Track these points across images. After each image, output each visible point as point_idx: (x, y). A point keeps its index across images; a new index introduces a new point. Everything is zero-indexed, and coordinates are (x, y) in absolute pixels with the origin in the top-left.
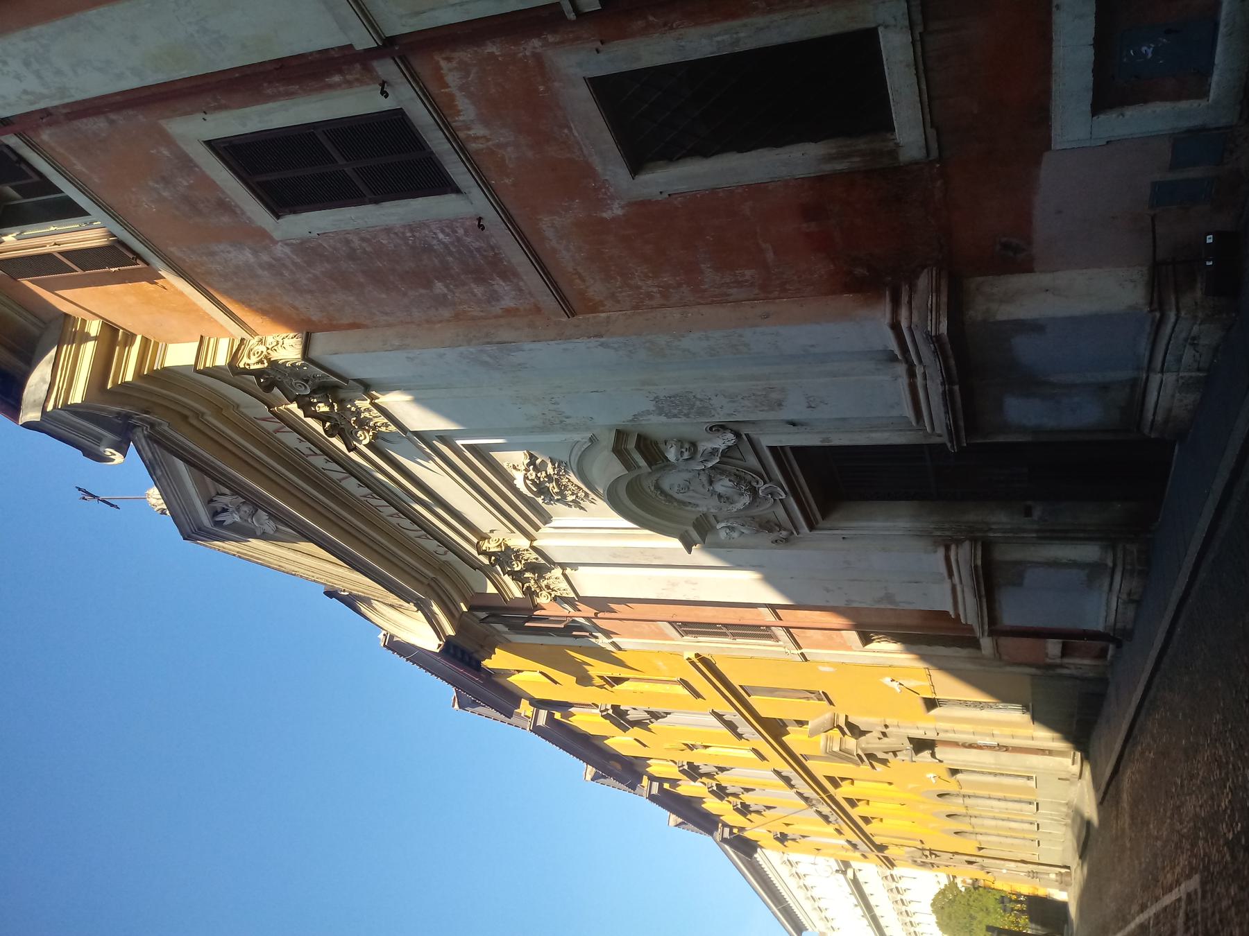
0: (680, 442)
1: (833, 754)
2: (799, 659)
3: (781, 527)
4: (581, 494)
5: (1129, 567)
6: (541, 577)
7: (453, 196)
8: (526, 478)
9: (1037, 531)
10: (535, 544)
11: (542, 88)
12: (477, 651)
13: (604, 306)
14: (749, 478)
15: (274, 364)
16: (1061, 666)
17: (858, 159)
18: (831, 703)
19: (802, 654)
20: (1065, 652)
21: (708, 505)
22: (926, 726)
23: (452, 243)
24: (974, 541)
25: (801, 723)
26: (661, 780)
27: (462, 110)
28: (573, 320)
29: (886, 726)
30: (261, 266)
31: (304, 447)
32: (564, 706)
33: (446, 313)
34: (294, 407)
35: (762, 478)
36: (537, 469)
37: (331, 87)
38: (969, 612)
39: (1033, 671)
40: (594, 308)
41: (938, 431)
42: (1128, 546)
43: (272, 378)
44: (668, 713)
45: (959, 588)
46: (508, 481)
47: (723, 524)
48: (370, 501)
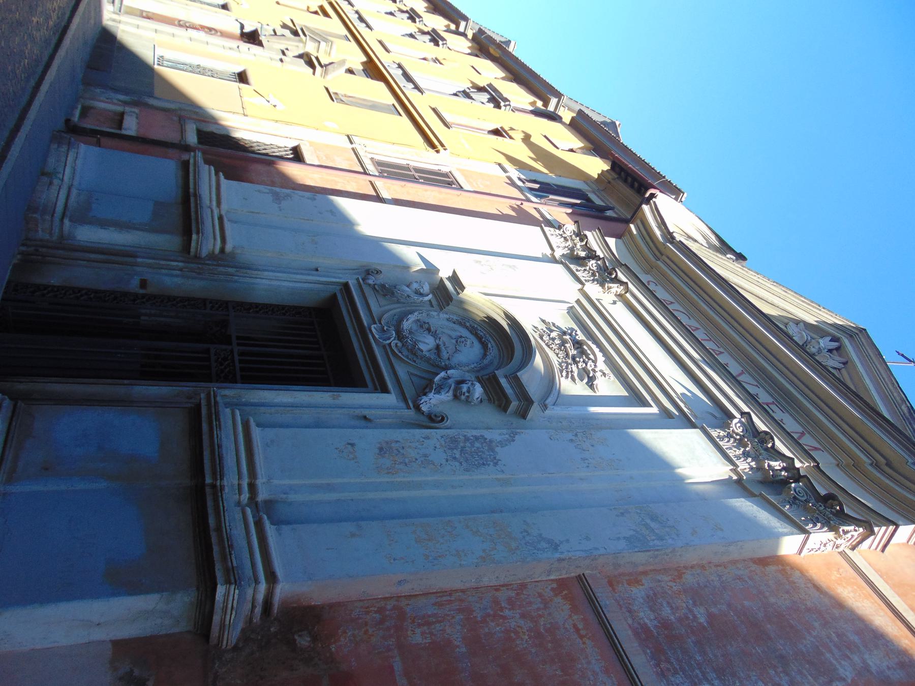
0: (468, 401)
1: (326, 40)
2: (354, 139)
3: (373, 287)
4: (546, 338)
5: (48, 217)
6: (572, 249)
8: (595, 362)
9: (137, 265)
10: (580, 286)
12: (614, 179)
13: (553, 589)
14: (405, 352)
15: (832, 529)
16: (125, 103)
18: (327, 89)
19: (351, 143)
20: (119, 119)
21: (439, 319)
22: (246, 57)
24: (197, 257)
25: (350, 71)
26: (457, 32)
28: (579, 572)
29: (281, 60)
31: (778, 415)
32: (537, 113)
33: (689, 579)
34: (798, 464)
35: (392, 351)
36: (585, 370)
38: (206, 177)
39: (152, 102)
40: (562, 584)
41: (228, 411)
42: (47, 237)
43: (828, 510)
44: (455, 95)
45: (214, 203)
46: (609, 361)
47: (426, 298)
48: (715, 348)
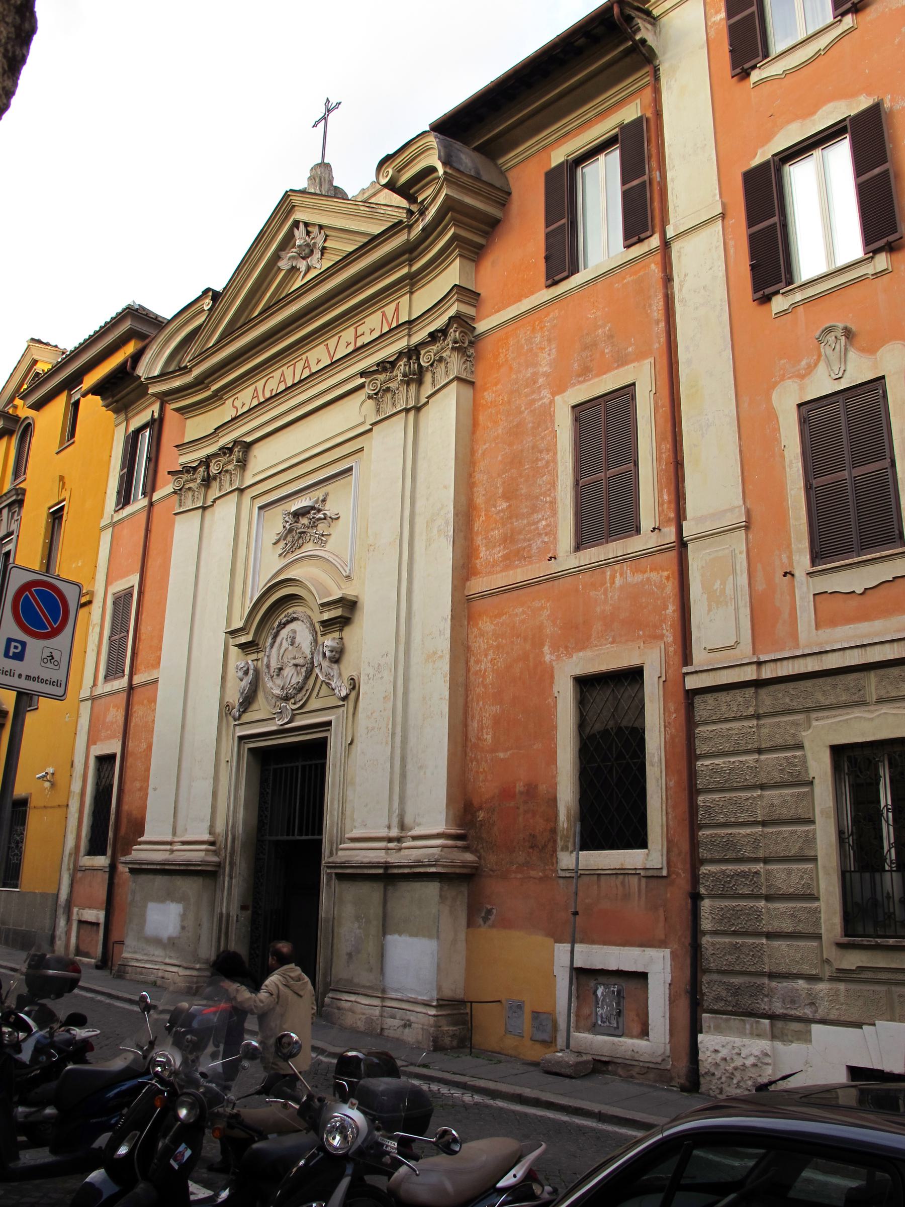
7: (573, 544)
9: (228, 915)
11: (641, 633)
14: (299, 696)
16: (69, 920)
17: (565, 826)
23: (537, 528)
27: (628, 565)
30: (535, 374)
37: (660, 492)
41: (340, 853)
